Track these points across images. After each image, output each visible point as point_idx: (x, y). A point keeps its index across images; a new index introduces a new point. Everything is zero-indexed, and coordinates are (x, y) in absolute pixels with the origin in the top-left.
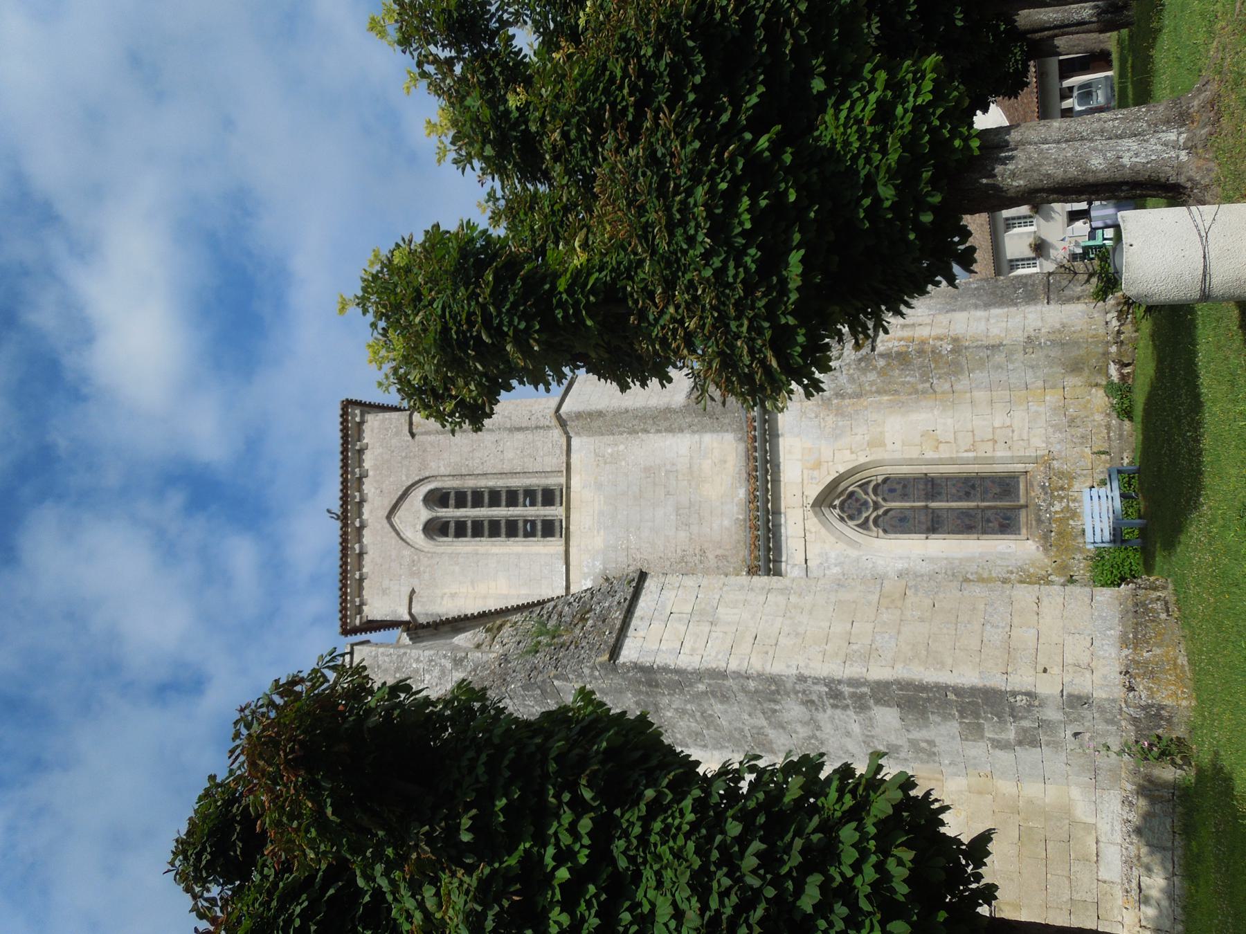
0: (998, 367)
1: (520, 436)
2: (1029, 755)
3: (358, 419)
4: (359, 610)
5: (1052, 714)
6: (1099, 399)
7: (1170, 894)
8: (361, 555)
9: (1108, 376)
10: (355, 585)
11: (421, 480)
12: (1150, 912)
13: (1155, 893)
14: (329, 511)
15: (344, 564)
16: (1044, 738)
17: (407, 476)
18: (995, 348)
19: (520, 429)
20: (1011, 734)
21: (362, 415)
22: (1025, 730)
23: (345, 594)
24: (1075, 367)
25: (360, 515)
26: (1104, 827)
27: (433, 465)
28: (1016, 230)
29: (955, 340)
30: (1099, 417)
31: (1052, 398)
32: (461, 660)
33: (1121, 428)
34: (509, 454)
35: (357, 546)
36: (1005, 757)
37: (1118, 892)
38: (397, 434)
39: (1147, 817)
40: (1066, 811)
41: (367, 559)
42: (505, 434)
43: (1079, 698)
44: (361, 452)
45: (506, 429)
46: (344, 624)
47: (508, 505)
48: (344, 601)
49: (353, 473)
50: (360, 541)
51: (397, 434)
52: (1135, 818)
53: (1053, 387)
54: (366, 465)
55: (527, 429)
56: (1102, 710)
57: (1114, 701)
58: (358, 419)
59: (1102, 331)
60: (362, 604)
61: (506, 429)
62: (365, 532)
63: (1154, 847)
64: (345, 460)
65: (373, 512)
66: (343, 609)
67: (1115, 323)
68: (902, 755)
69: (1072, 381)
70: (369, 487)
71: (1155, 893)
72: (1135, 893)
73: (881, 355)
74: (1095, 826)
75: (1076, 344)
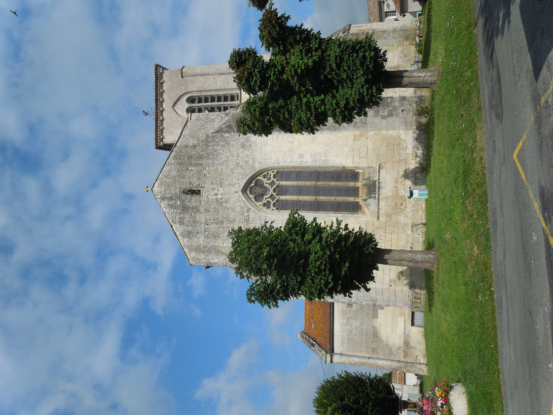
0: (385, 38)
1: (223, 76)
2: (390, 120)
3: (161, 72)
4: (162, 140)
5: (397, 104)
6: (413, 48)
7: (423, 154)
8: (162, 121)
9: (416, 41)
10: (160, 131)
11: (185, 93)
12: (418, 159)
13: (419, 154)
14: (144, 112)
15: (157, 123)
16: (394, 113)
17: (180, 92)
18: (384, 32)
19: (223, 74)
20: (386, 113)
21: (163, 70)
22: (390, 111)
23: (157, 136)
24: (407, 38)
25: (162, 106)
26: (408, 140)
27: (190, 87)
28: (389, 17)
29: (373, 30)
30: (413, 54)
31: (400, 49)
32: (228, 114)
33: (419, 57)
34: (219, 83)
35: (161, 117)
36: (384, 121)
37: (411, 156)
38: (176, 77)
39: (418, 135)
40: (399, 137)
41: (165, 122)
42: (218, 76)
43: (403, 97)
44: (162, 83)
45: (218, 74)
46: (156, 145)
47: (218, 101)
48: (157, 136)
49: (160, 91)
50: (162, 115)
51: (176, 77)
52: (415, 136)
53: (400, 45)
54: (164, 88)
55: (226, 74)
56: (409, 101)
57: (412, 97)
58: (161, 72)
59: (415, 26)
60: (163, 138)
61: (218, 74)
62: (164, 112)
63: (420, 142)
64: (156, 85)
65: (167, 105)
66: (156, 139)
67: (418, 24)
68: (358, 125)
69: (406, 43)
70: (165, 96)
71: (419, 154)
72: (415, 155)
73: (351, 34)
74: (406, 140)
75: (407, 30)
